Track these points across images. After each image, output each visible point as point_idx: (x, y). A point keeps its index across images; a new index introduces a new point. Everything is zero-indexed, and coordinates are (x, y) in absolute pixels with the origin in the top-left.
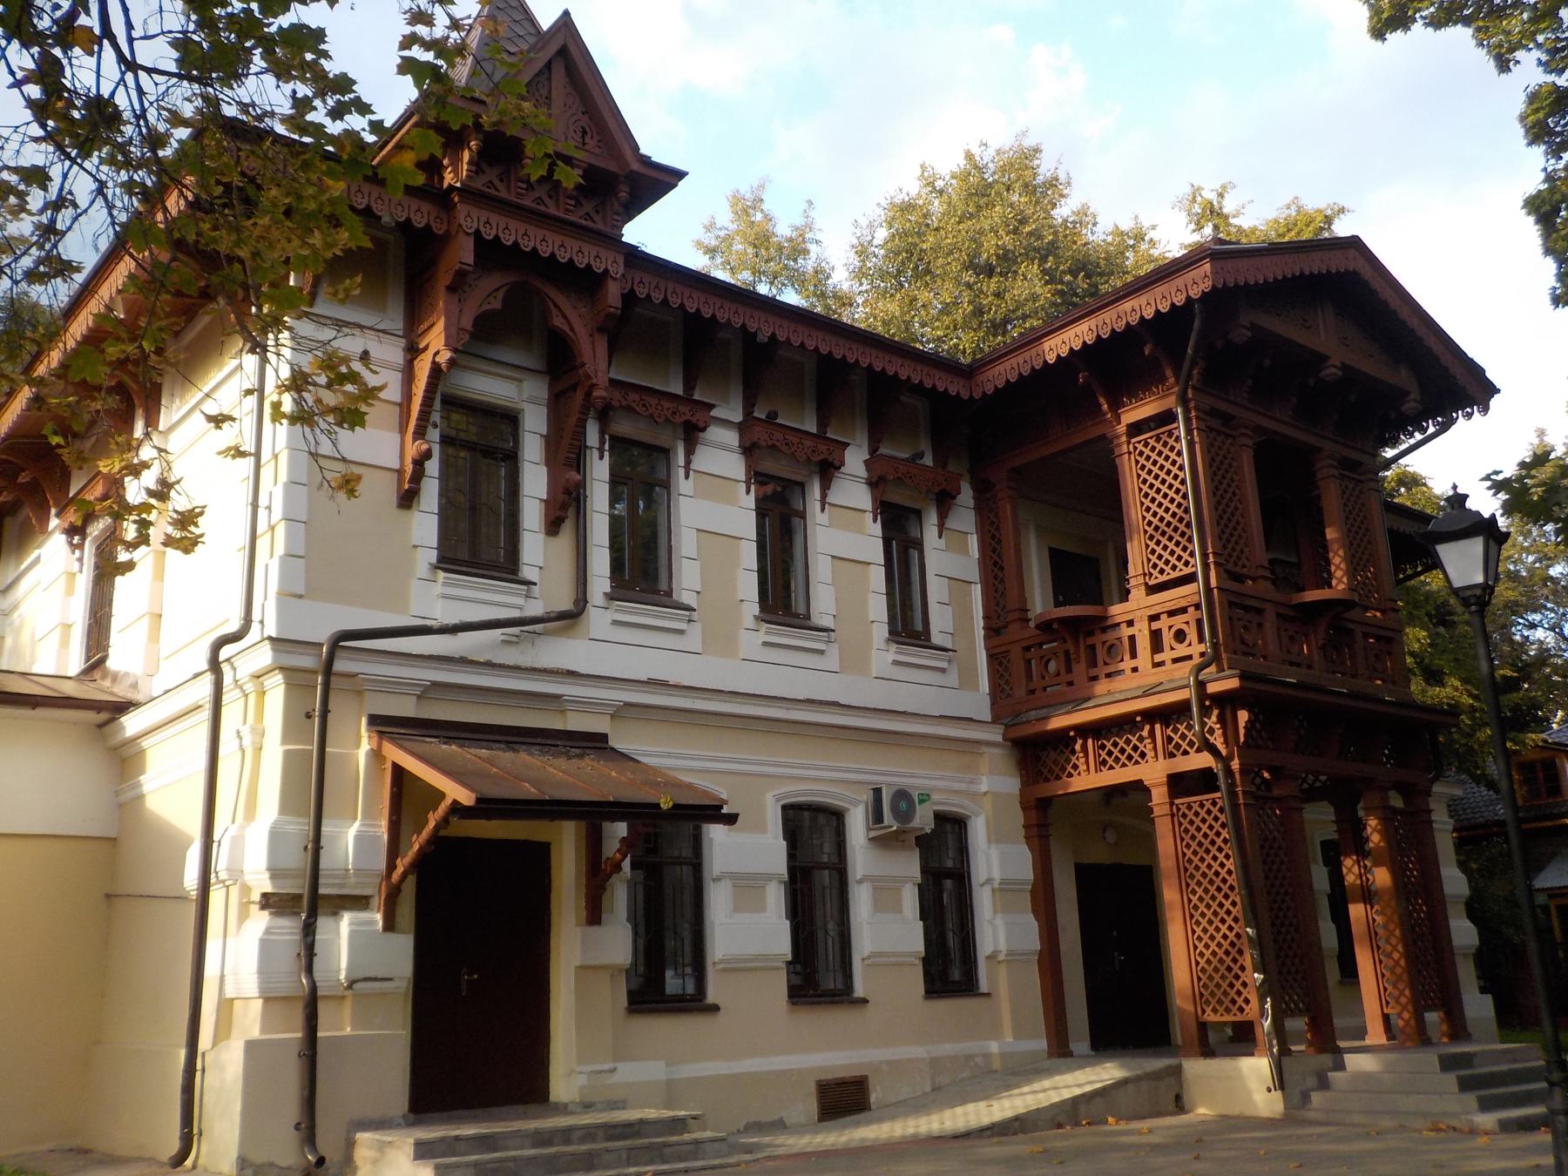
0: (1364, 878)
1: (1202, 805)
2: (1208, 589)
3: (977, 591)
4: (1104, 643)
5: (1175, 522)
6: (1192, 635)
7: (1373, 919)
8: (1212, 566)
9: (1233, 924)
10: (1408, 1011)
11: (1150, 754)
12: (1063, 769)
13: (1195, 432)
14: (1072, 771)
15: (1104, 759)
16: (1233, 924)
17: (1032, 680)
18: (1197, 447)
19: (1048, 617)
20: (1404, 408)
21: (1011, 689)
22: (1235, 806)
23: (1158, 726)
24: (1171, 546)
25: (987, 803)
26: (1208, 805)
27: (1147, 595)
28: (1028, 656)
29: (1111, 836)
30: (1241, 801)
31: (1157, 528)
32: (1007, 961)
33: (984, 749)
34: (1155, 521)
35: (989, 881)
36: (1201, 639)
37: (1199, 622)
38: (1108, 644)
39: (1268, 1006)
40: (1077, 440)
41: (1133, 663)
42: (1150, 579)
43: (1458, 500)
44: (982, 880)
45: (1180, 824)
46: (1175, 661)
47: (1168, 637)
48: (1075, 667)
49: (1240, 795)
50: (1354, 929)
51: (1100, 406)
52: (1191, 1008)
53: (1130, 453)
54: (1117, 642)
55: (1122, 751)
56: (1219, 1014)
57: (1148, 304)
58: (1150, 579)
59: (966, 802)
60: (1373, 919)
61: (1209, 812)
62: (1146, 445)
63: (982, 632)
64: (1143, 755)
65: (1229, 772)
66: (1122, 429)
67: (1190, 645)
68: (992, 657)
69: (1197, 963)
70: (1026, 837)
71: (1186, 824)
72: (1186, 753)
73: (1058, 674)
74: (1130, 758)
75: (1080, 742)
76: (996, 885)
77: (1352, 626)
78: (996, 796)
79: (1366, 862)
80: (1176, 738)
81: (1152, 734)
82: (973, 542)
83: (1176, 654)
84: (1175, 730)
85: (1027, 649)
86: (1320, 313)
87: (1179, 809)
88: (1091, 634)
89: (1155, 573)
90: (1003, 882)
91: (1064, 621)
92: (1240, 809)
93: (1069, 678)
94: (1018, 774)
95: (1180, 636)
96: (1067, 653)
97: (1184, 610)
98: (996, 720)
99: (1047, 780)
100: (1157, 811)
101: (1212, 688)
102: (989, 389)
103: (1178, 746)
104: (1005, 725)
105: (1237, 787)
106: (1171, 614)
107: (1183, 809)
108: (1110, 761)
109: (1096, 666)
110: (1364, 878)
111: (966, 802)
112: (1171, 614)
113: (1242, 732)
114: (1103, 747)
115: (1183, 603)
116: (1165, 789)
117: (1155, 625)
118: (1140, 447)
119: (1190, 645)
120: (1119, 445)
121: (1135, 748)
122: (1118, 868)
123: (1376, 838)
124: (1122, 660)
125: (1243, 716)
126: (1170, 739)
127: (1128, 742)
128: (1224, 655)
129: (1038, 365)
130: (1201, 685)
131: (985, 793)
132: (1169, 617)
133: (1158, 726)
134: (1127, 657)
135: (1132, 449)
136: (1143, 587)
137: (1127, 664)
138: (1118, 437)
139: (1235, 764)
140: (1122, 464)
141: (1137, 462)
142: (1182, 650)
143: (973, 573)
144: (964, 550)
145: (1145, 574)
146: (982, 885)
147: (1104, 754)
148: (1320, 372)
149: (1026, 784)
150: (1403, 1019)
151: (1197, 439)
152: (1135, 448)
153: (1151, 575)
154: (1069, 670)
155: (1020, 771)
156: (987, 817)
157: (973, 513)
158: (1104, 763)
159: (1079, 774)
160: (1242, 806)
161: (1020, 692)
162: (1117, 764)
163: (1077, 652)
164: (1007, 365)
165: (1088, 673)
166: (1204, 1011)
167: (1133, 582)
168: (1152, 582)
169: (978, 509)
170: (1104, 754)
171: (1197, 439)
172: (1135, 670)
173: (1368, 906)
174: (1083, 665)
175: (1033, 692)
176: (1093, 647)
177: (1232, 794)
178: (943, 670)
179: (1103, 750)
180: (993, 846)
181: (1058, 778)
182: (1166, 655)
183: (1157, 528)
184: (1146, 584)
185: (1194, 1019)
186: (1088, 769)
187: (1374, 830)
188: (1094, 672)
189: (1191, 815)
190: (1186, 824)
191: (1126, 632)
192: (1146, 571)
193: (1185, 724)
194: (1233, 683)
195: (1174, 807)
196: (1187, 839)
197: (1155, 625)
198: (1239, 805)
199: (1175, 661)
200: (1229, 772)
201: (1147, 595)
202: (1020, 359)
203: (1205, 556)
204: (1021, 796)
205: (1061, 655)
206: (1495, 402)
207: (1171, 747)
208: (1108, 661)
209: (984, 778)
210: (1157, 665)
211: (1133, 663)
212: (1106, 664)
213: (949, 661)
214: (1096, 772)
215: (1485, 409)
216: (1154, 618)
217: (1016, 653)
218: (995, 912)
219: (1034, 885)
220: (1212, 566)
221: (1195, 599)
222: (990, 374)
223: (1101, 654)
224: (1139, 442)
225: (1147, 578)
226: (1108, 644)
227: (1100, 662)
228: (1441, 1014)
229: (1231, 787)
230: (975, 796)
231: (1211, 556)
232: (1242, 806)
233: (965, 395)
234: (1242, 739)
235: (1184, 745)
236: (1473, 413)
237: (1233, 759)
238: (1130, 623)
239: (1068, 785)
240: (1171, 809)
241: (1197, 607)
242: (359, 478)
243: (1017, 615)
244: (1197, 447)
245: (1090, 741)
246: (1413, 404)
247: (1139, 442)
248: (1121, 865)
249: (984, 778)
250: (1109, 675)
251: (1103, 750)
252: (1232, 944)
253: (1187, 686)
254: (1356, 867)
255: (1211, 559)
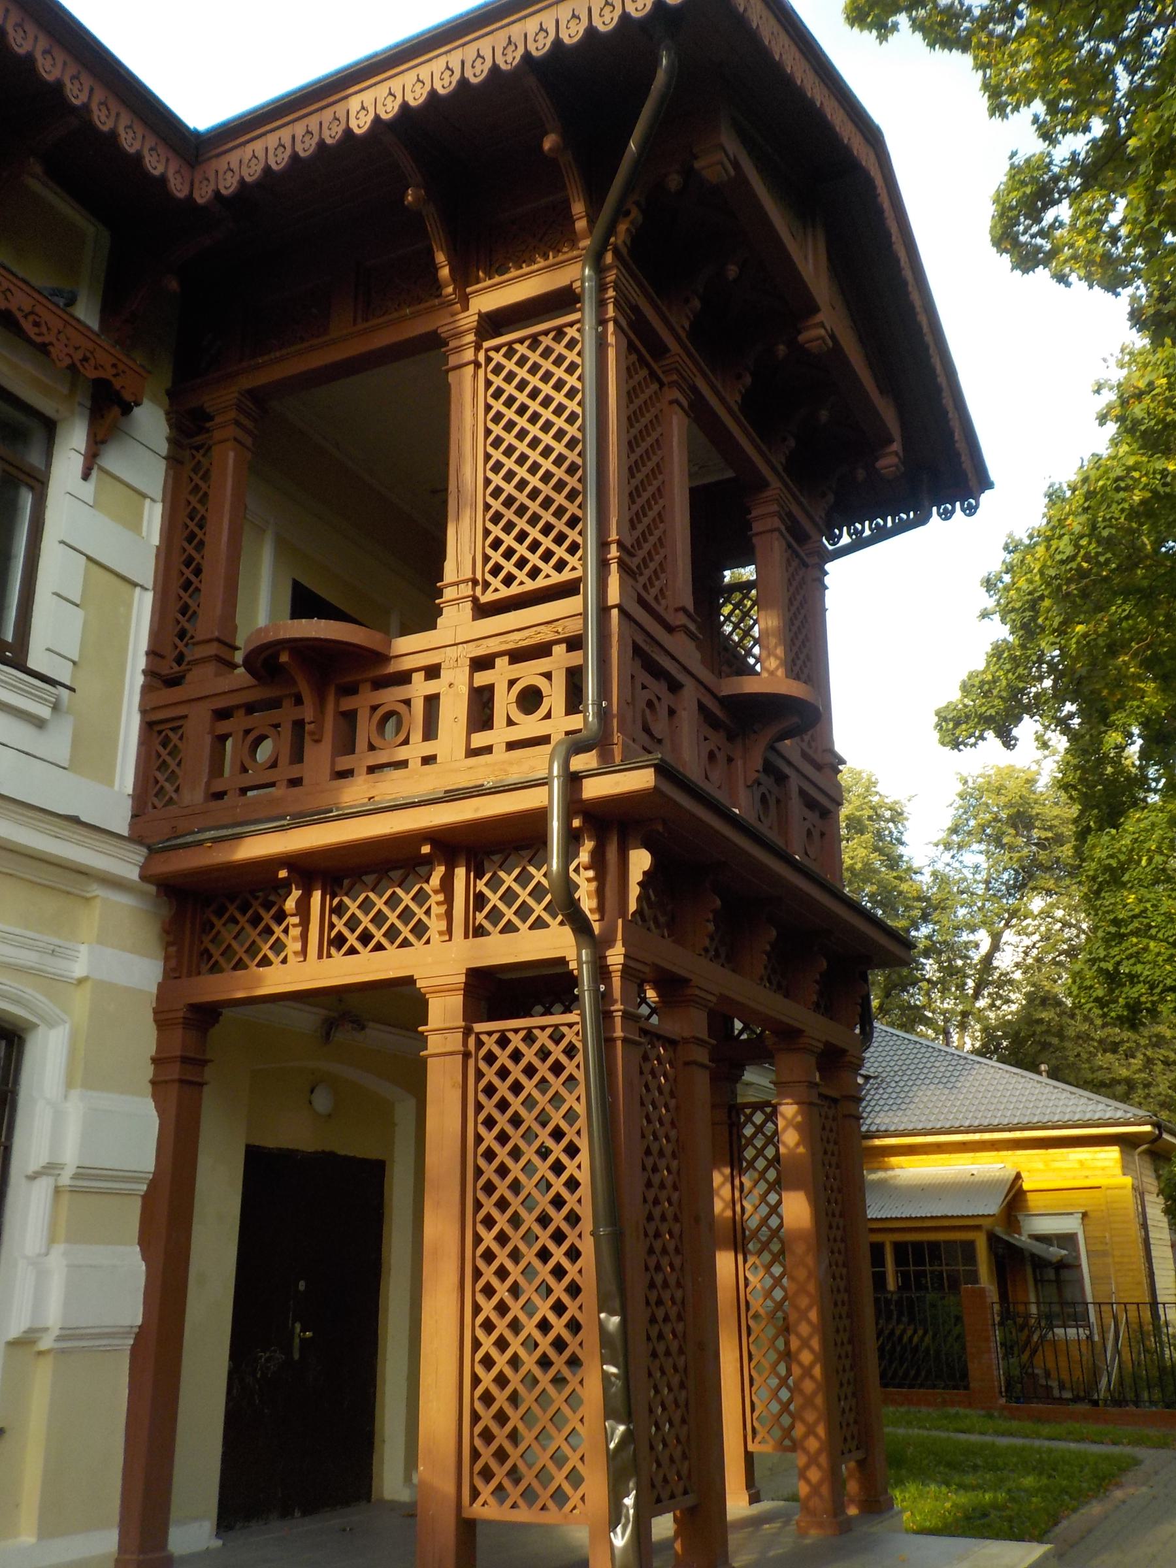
0: (738, 1208)
1: (529, 1038)
2: (603, 610)
3: (143, 605)
4: (374, 708)
5: (546, 490)
6: (555, 696)
7: (746, 1278)
8: (614, 567)
9: (566, 1299)
10: (819, 1466)
11: (435, 925)
12: (253, 950)
13: (611, 327)
14: (270, 955)
15: (340, 933)
16: (566, 1299)
17: (221, 774)
18: (611, 353)
19: (271, 637)
20: (880, 464)
21: (177, 790)
22: (605, 1042)
23: (460, 872)
24: (534, 533)
25: (81, 1001)
26: (543, 1038)
27: (474, 620)
28: (224, 727)
29: (322, 1101)
30: (619, 1033)
31: (509, 502)
32: (63, 1351)
33: (97, 890)
34: (509, 489)
35: (51, 1169)
36: (574, 702)
37: (574, 677)
38: (380, 712)
39: (629, 1501)
40: (384, 339)
41: (428, 748)
42: (484, 592)
43: (1021, 540)
44: (34, 1166)
45: (480, 1075)
46: (511, 746)
47: (504, 702)
48: (310, 750)
49: (618, 1021)
50: (720, 1295)
51: (435, 269)
52: (449, 1488)
53: (477, 365)
54: (401, 708)
55: (379, 919)
56: (509, 1503)
57: (574, 16)
58: (484, 592)
59: (31, 993)
60: (746, 1278)
61: (544, 1054)
62: (509, 355)
63: (140, 680)
64: (420, 930)
65: (601, 971)
66: (468, 319)
67: (548, 716)
68: (150, 727)
69: (476, 1381)
70: (153, 1083)
71: (490, 1074)
72: (510, 928)
73: (274, 765)
74: (392, 934)
75: (296, 894)
76: (65, 1179)
77: (787, 770)
78: (103, 989)
79: (744, 1179)
80: (494, 899)
81: (447, 886)
82: (153, 516)
83: (516, 734)
84: (494, 884)
85: (222, 714)
86: (810, 244)
87: (480, 1044)
88: (351, 690)
89: (496, 582)
90: (82, 1173)
91: (305, 649)
92: (615, 1047)
93: (295, 771)
94: (161, 954)
95: (530, 699)
96: (299, 725)
97: (542, 650)
98: (136, 837)
99: (215, 968)
100: (435, 1044)
101: (593, 789)
102: (229, 185)
103: (495, 915)
104: (149, 848)
105: (614, 1002)
106: (518, 656)
107: (490, 1043)
108: (352, 939)
109: (353, 752)
110: (738, 1208)
111: (31, 993)
112: (518, 656)
113: (634, 891)
114: (339, 910)
115: (546, 635)
116: (457, 1000)
117: (482, 679)
118: (498, 357)
119: (548, 716)
120: (459, 349)
121: (406, 915)
122: (326, 1161)
123: (790, 1138)
124: (406, 742)
125: (640, 861)
126: (481, 900)
127: (393, 902)
128: (617, 737)
129: (332, 135)
130: (573, 780)
131: (81, 981)
132: (512, 662)
133: (460, 872)
134: (417, 735)
135: (481, 358)
136: (469, 605)
137: (416, 749)
138: (459, 335)
139: (616, 957)
140: (460, 383)
141: (488, 383)
142: (529, 726)
143: (144, 568)
144: (134, 524)
145: (475, 582)
146: (33, 1177)
147: (340, 925)
148: (799, 333)
149: (173, 974)
150: (808, 1481)
151: (611, 339)
152: (489, 360)
153: (487, 585)
154: (298, 756)
155: (168, 944)
156: (73, 1036)
157: (162, 465)
158: (339, 941)
159: (284, 961)
160: (619, 1043)
161: (193, 795)
162: (365, 945)
163: (319, 721)
164: (272, 140)
165: (333, 763)
166: (475, 1494)
167: (449, 593)
168: (487, 597)
169: (174, 460)
170: (340, 925)
171: (611, 339)
172: (428, 760)
173: (740, 1258)
174: (326, 746)
175: (219, 796)
176: (350, 717)
177: (604, 1016)
178: (39, 723)
179: (340, 917)
180: (75, 1094)
181: (240, 965)
182: (498, 735)
183: (509, 502)
184: (475, 600)
185: (453, 1505)
186: (304, 951)
187: (790, 1123)
188: (344, 763)
189: (503, 1057)
190: (490, 1074)
191: (420, 688)
192: (479, 577)
193: (517, 871)
194: (641, 779)
195: (472, 1040)
196: (490, 1106)
197: (482, 679)
198: (614, 1040)
199: (511, 746)
200: (601, 971)
201: (474, 620)
202: (299, 129)
203: (603, 545)
204: (158, 998)
205: (286, 731)
206: (986, 497)
207: (480, 917)
208: (376, 742)
209: (84, 949)
210: (472, 753)
211: (428, 748)
212: (372, 748)
213: (56, 707)
214: (320, 957)
215: (971, 511)
216: (482, 663)
217: (199, 723)
218: (52, 1240)
219: (153, 1184)
220: (614, 567)
221: (572, 628)
222: (233, 158)
223: (365, 729)
224: (497, 349)
225: (479, 589)
226: (380, 712)
227: (361, 743)
228: (900, 1482)
229: (603, 1000)
230: (54, 983)
231: (614, 547)
232: (619, 1043)
233: (178, 187)
234: (633, 906)
235: (509, 914)
236: (953, 511)
237: (610, 943)
238: (433, 672)
239: (259, 981)
240: (465, 1043)
241: (575, 643)
242: (751, 1502)
243: (212, 649)
244: (611, 353)
245: (317, 896)
246: (894, 460)
247: (497, 349)
248: (332, 1154)
249: (84, 949)
250: (371, 770)
251: (340, 917)
252: (559, 1344)
253: (544, 782)
254: (728, 1186)
255: (614, 551)
